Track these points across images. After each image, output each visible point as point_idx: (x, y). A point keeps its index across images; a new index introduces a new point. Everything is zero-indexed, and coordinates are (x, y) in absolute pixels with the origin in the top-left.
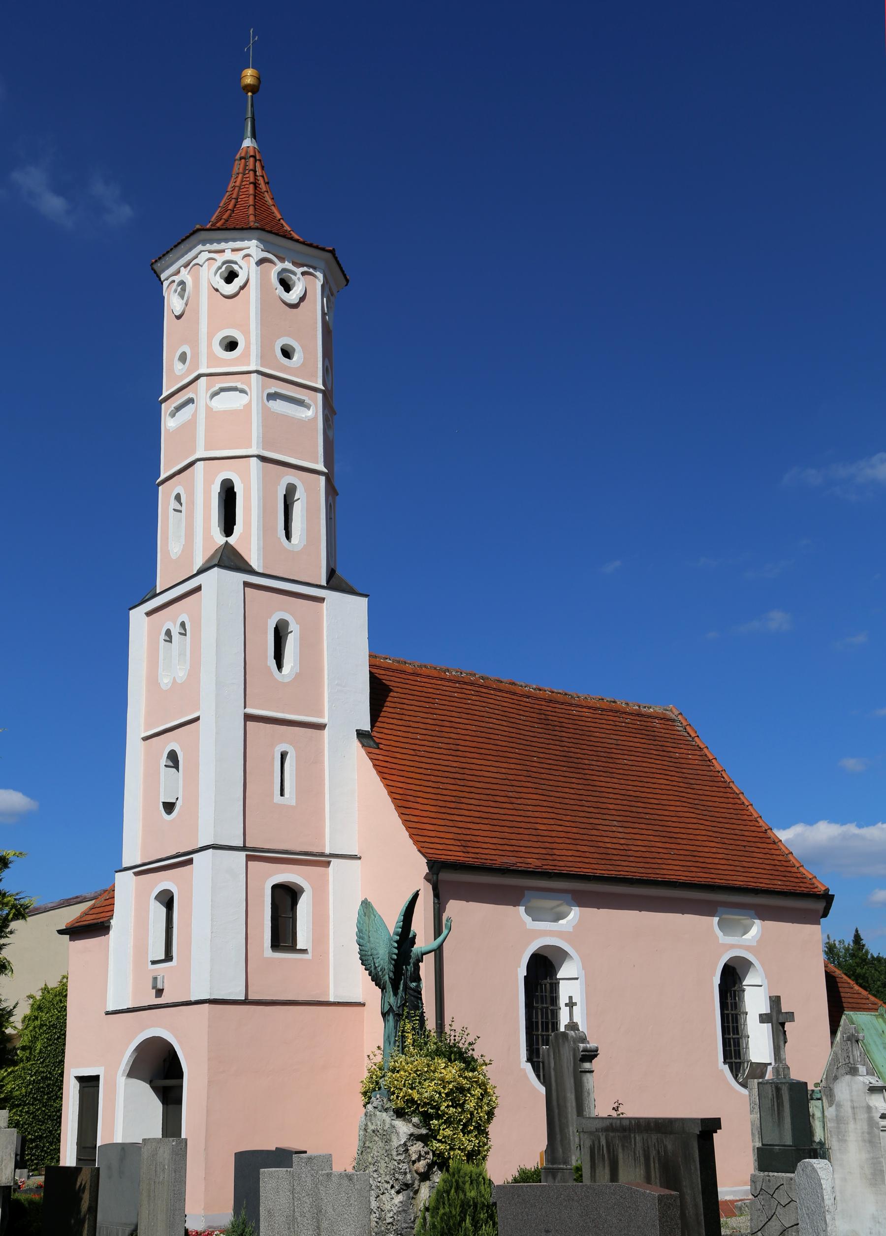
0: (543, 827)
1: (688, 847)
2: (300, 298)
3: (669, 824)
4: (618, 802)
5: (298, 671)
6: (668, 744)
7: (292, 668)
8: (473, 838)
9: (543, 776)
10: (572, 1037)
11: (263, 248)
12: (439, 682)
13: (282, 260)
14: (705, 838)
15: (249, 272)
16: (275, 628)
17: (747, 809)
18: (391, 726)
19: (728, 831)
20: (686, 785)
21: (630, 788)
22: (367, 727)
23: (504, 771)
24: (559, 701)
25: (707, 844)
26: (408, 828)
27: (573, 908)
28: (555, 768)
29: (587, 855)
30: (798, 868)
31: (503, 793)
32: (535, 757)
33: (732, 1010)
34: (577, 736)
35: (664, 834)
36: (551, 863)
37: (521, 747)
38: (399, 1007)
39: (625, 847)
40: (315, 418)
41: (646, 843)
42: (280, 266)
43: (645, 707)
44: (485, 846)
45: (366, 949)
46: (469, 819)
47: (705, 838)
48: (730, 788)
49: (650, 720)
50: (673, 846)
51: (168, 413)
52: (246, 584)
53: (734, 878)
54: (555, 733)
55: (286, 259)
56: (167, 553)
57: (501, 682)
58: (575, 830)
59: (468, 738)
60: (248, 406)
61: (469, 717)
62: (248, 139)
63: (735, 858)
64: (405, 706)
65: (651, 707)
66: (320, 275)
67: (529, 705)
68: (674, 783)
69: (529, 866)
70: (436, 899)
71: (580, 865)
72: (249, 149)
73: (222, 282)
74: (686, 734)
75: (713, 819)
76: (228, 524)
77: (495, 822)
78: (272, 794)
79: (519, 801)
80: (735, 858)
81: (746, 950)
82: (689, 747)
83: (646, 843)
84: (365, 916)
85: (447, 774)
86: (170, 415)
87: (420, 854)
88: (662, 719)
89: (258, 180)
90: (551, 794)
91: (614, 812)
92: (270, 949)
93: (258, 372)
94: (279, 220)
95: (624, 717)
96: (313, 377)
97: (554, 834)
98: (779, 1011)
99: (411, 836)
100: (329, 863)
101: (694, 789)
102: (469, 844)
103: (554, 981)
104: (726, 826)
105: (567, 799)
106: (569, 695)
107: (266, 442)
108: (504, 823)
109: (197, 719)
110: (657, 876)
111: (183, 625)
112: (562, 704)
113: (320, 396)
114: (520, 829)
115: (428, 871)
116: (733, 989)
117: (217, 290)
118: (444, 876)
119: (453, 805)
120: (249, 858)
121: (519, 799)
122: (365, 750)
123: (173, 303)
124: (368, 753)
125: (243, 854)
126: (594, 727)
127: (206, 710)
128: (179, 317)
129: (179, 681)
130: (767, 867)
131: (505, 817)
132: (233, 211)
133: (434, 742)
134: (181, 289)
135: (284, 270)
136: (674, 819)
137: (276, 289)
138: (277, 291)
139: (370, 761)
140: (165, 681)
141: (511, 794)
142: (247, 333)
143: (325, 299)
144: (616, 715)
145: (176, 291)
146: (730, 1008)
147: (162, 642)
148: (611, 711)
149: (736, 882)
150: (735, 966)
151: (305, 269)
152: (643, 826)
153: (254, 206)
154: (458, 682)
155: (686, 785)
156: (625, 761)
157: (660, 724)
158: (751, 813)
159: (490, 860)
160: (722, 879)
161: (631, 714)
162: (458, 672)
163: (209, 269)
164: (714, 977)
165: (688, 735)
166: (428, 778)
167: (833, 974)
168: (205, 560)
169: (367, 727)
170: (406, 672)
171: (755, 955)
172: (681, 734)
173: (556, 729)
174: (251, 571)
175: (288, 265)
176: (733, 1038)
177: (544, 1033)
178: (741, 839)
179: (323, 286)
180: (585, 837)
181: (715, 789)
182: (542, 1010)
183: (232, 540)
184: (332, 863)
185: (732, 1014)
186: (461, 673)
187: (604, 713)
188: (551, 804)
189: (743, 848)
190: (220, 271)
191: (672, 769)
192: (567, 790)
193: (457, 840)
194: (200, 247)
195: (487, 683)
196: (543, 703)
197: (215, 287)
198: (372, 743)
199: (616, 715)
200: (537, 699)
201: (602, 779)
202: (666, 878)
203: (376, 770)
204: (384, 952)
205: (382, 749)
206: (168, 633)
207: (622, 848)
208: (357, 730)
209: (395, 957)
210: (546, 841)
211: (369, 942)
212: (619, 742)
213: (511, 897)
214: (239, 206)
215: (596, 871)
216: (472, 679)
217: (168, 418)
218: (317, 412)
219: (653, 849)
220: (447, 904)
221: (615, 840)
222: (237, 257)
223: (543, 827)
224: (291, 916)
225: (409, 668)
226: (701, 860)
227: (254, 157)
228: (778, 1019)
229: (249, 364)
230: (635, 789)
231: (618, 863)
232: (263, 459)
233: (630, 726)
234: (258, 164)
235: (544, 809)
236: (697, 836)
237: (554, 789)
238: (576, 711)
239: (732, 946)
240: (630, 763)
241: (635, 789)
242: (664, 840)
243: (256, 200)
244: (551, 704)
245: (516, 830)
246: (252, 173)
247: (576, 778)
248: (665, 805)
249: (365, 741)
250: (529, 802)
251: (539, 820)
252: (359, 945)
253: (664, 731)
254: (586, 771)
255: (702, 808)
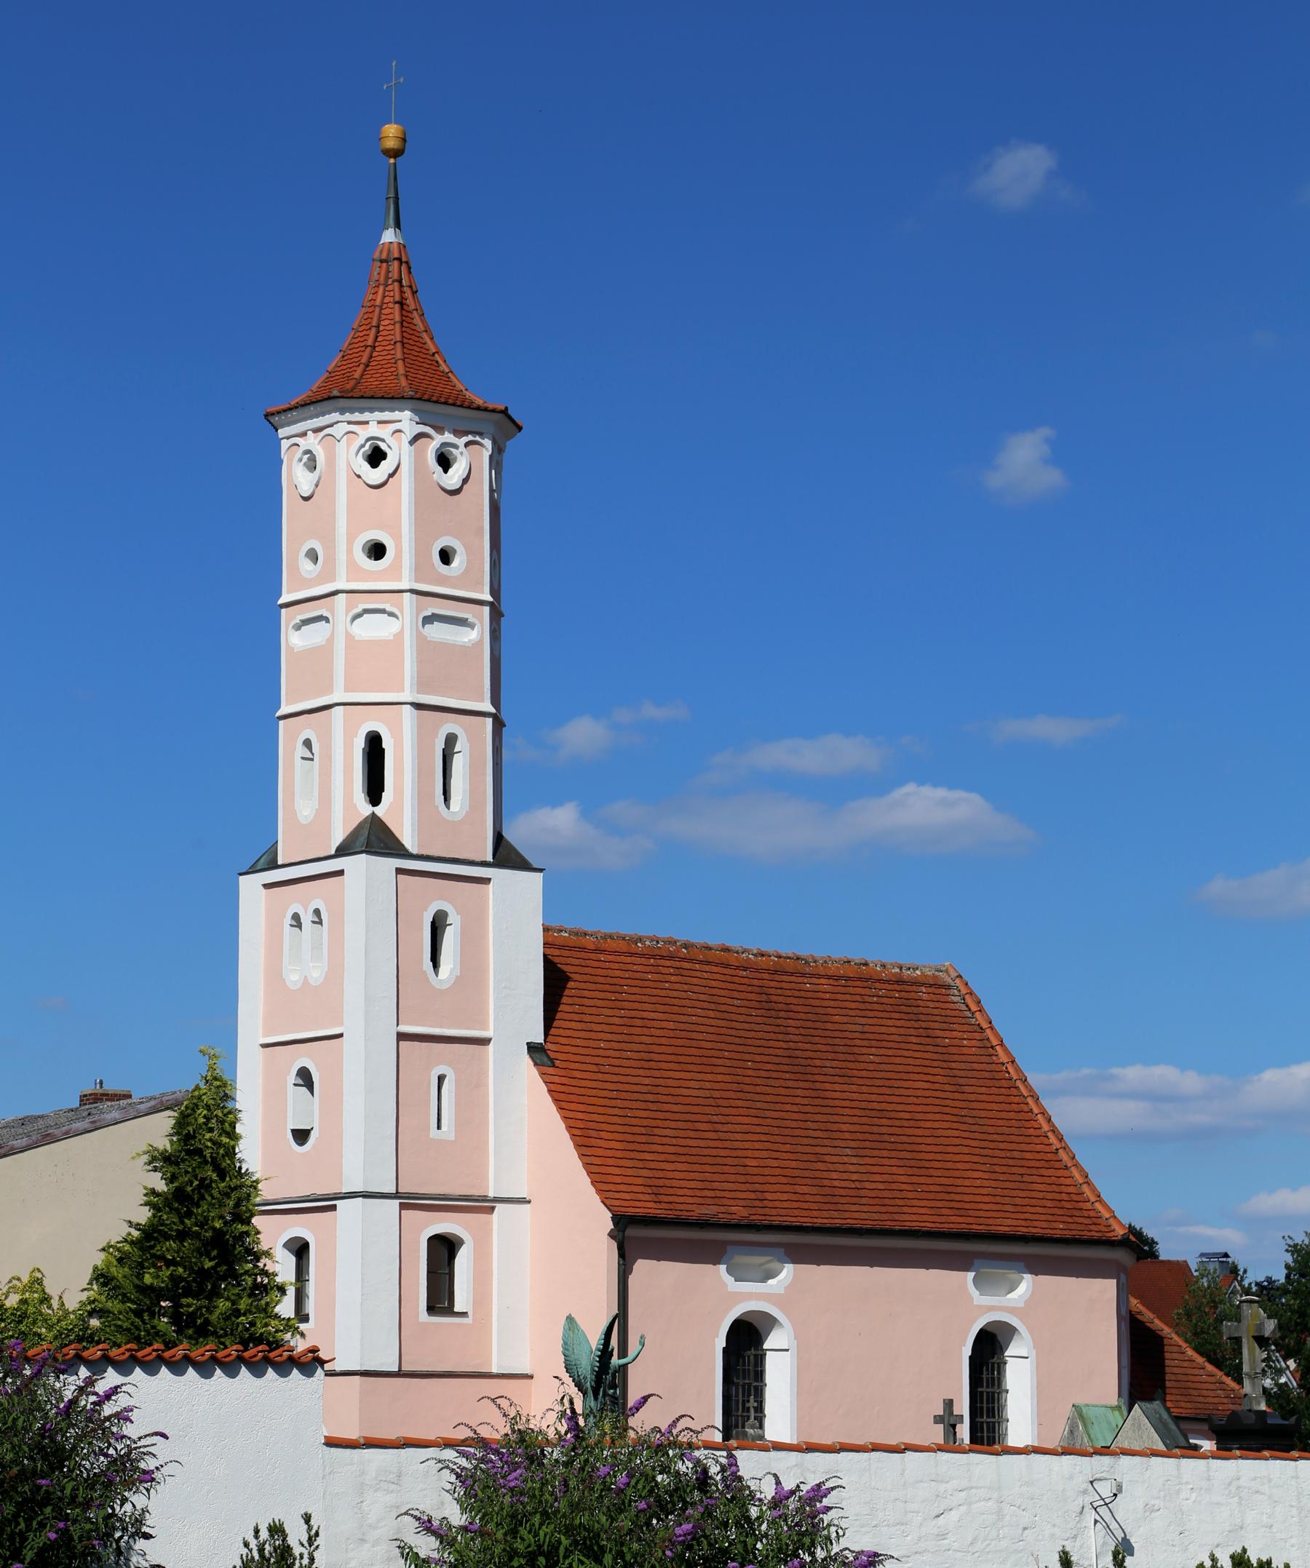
0: (754, 1163)
1: (943, 1181)
2: (464, 480)
3: (923, 1148)
4: (855, 1120)
5: (459, 974)
6: (936, 1025)
7: (452, 970)
8: (668, 1183)
9: (758, 1089)
10: (751, 1434)
11: (418, 420)
12: (629, 960)
13: (440, 430)
14: (967, 1166)
15: (400, 454)
16: (432, 922)
17: (1035, 1119)
18: (568, 1033)
19: (1003, 1154)
20: (953, 1088)
21: (873, 1097)
22: (539, 1038)
23: (708, 1085)
24: (788, 970)
25: (970, 1174)
26: (590, 1173)
27: (786, 1265)
28: (775, 1075)
29: (807, 1198)
30: (1093, 1203)
31: (705, 1118)
32: (749, 1061)
33: (988, 1387)
34: (809, 1024)
35: (913, 1163)
36: (760, 1211)
37: (733, 1047)
38: (599, 1411)
39: (857, 1184)
40: (481, 641)
41: (886, 1178)
42: (438, 440)
43: (909, 969)
44: (680, 1192)
45: (571, 1359)
46: (662, 1157)
47: (967, 1166)
48: (1016, 1088)
49: (914, 988)
50: (922, 1180)
51: (291, 626)
52: (399, 871)
53: (999, 1221)
54: (779, 1022)
55: (446, 429)
56: (292, 813)
57: (711, 949)
58: (794, 1164)
59: (664, 1041)
60: (400, 635)
61: (667, 1008)
62: (390, 229)
63: (1006, 1192)
64: (586, 1002)
65: (917, 968)
66: (488, 443)
67: (746, 981)
68: (937, 1087)
69: (734, 1216)
70: (621, 1259)
71: (796, 1212)
72: (392, 245)
73: (366, 466)
74: (964, 1007)
75: (984, 1136)
76: (375, 790)
77: (694, 1159)
78: (428, 1128)
79: (725, 1128)
80: (1006, 1192)
81: (1008, 1312)
82: (965, 1028)
83: (886, 1178)
84: (570, 1330)
85: (636, 1096)
86: (293, 627)
87: (604, 1206)
88: (931, 986)
89: (405, 293)
90: (768, 1114)
91: (847, 1136)
92: (426, 1313)
93: (412, 591)
94: (434, 354)
95: (877, 987)
96: (477, 586)
97: (766, 1171)
98: (951, 1413)
99: (593, 1183)
100: (493, 1208)
101: (964, 1093)
102: (662, 1191)
103: (761, 1352)
104: (1002, 1146)
105: (787, 1120)
106: (802, 960)
107: (423, 683)
108: (705, 1160)
109: (341, 1035)
110: (894, 1223)
111: (317, 912)
112: (792, 974)
113: (486, 609)
114: (724, 1167)
115: (613, 1227)
116: (991, 1361)
117: (359, 476)
118: (631, 1232)
119: (643, 1139)
120: (403, 1207)
121: (725, 1125)
122: (538, 1070)
123: (296, 477)
124: (542, 1074)
125: (397, 1202)
126: (833, 1008)
127: (352, 1026)
128: (306, 499)
129: (312, 982)
130: (1049, 1204)
131: (706, 1152)
132: (375, 347)
133: (621, 1050)
134: (308, 459)
135: (444, 445)
136: (929, 1140)
137: (434, 473)
138: (435, 475)
139: (543, 1084)
140: (293, 978)
141: (715, 1119)
142: (397, 538)
143: (493, 471)
144: (866, 984)
145: (300, 460)
146: (985, 1384)
147: (287, 928)
148: (860, 979)
149: (1000, 1228)
150: (996, 1332)
151: (470, 438)
152: (885, 1153)
153: (404, 360)
154: (653, 957)
155: (953, 1088)
156: (871, 1057)
157: (928, 993)
158: (1040, 1125)
159: (687, 1211)
160: (982, 1225)
161: (888, 982)
162: (652, 941)
163: (348, 446)
164: (963, 1348)
165: (966, 1009)
166: (613, 1103)
167: (1160, 1333)
168: (346, 836)
169: (539, 1038)
170: (585, 949)
171: (1021, 1320)
172: (957, 1007)
173: (780, 1016)
174: (406, 855)
175: (448, 437)
176: (987, 1422)
177: (744, 1414)
178: (1020, 1165)
179: (491, 457)
180: (807, 1174)
181: (994, 1090)
182: (743, 1386)
183: (380, 811)
184: (496, 1209)
185: (988, 1393)
186: (658, 942)
187: (850, 983)
188: (766, 1129)
189: (1019, 1178)
190: (363, 450)
191: (935, 1064)
192: (788, 1107)
193: (648, 1186)
194: (335, 416)
195: (691, 953)
196: (766, 976)
197: (357, 473)
198: (545, 1059)
199: (866, 984)
200: (757, 970)
201: (837, 1087)
202: (905, 1226)
203: (552, 1097)
204: (587, 1365)
205: (558, 1067)
206: (296, 917)
207: (854, 1186)
208: (527, 1043)
209: (597, 1369)
210: (756, 1181)
211: (574, 1353)
212: (867, 1028)
213: (711, 1254)
214: (381, 348)
215: (816, 1220)
216: (671, 949)
217: (291, 631)
218: (482, 633)
219: (894, 1186)
220: (634, 1264)
221: (845, 1176)
222: (385, 432)
223: (754, 1163)
224: (447, 1272)
225: (589, 942)
226: (958, 1197)
227: (399, 259)
228: (949, 1421)
229: (400, 579)
230: (881, 1098)
231: (846, 1208)
232: (419, 706)
233: (885, 1000)
234: (404, 267)
235: (756, 1137)
236: (957, 1164)
237: (772, 1106)
238: (809, 984)
239: (991, 1309)
240: (877, 1059)
241: (881, 1098)
242: (910, 1171)
243: (404, 329)
244: (776, 977)
245: (719, 1169)
246: (396, 284)
247: (802, 1089)
248: (919, 1120)
249: (537, 1055)
250: (738, 1128)
251: (749, 1153)
252: (565, 1356)
253: (931, 1005)
254: (816, 1078)
255: (971, 1121)
